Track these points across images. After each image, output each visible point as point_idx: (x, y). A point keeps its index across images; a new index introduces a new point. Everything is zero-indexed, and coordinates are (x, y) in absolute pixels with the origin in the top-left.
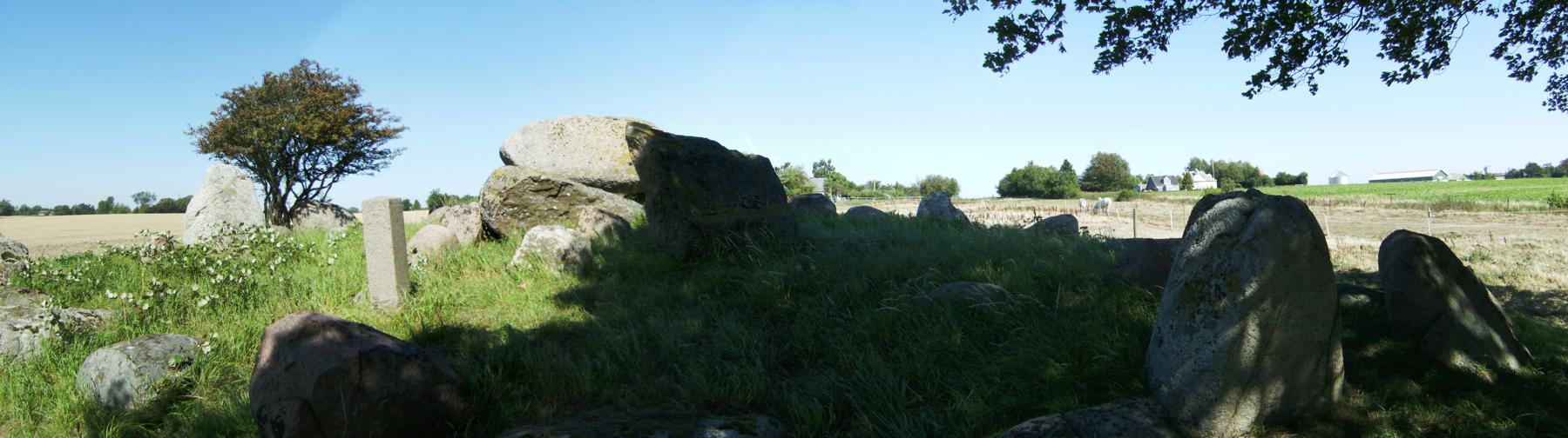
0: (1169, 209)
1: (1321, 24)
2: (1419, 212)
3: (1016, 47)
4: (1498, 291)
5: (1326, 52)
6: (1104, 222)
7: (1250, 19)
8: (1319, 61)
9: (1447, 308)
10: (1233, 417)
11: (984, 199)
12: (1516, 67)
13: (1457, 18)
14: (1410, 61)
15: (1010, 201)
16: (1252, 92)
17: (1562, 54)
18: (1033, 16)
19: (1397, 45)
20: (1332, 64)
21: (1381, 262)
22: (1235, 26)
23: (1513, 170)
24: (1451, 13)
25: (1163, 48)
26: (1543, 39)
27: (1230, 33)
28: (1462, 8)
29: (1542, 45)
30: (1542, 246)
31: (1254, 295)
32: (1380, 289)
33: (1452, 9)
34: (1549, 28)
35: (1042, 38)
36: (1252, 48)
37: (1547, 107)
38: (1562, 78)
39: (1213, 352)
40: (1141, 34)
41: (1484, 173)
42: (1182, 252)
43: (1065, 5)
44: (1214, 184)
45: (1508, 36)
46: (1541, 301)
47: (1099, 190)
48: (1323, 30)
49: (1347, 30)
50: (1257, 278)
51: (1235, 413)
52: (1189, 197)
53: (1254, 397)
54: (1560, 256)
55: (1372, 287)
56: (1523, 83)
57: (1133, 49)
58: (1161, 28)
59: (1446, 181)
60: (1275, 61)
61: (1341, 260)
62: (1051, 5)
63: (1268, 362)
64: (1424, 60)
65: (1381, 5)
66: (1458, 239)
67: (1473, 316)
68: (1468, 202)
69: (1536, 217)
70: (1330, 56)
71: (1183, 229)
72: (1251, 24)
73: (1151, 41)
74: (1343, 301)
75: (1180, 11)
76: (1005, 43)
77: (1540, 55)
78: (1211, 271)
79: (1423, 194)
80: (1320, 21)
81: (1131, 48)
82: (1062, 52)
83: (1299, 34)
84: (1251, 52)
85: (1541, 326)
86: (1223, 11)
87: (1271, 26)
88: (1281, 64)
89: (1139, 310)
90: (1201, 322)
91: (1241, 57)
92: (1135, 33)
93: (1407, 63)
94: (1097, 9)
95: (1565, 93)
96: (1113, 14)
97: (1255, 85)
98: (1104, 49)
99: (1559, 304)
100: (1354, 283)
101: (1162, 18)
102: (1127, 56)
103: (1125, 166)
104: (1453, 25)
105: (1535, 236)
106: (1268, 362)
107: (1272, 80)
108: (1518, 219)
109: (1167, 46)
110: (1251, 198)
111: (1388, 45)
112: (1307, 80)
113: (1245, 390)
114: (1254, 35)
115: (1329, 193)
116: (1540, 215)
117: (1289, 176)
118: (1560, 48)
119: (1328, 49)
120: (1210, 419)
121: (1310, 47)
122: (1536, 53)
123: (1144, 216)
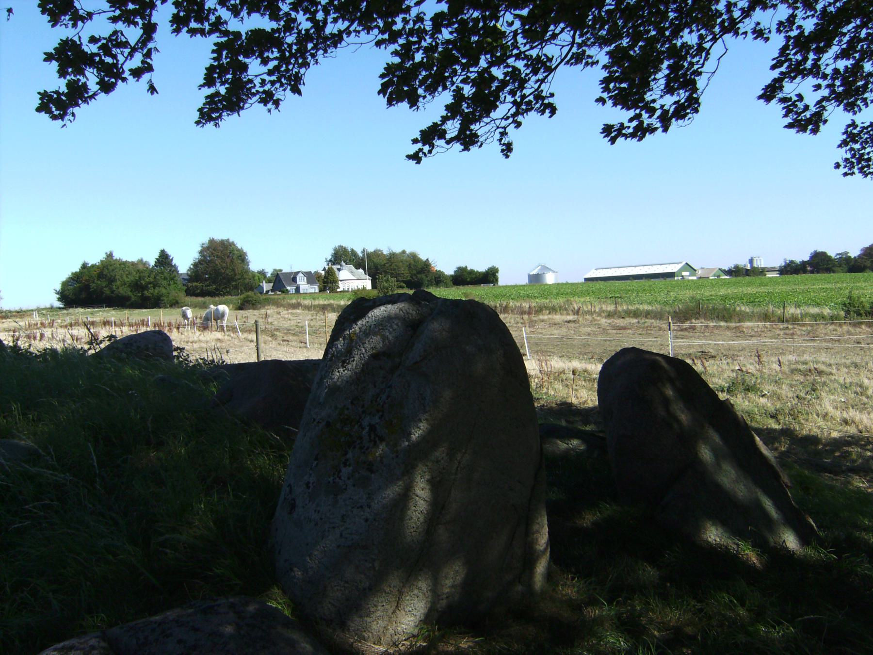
0: (305, 319)
1: (518, 57)
2: (656, 323)
3: (85, 85)
4: (770, 436)
5: (523, 97)
6: (218, 340)
7: (418, 50)
8: (514, 110)
9: (696, 461)
10: (393, 612)
11: (38, 310)
12: (796, 113)
13: (710, 44)
14: (642, 109)
15: (80, 313)
16: (421, 154)
17: (864, 92)
18: (109, 40)
19: (624, 85)
20: (533, 114)
21: (602, 392)
22: (397, 60)
23: (792, 262)
24: (701, 37)
25: (296, 90)
26: (836, 71)
27: (390, 69)
28: (717, 29)
29: (833, 79)
30: (834, 371)
31: (423, 438)
32: (601, 432)
33: (703, 32)
34: (844, 54)
35: (123, 72)
36: (420, 91)
37: (842, 170)
38: (864, 128)
39: (366, 520)
40: (265, 69)
41: (749, 267)
42: (322, 379)
43: (156, 24)
44: (368, 284)
45: (783, 69)
46: (833, 452)
47: (212, 294)
48: (520, 64)
49: (554, 64)
50: (426, 416)
51: (397, 607)
52: (332, 301)
53: (423, 585)
54: (861, 386)
55: (588, 428)
56: (807, 136)
57: (254, 91)
58: (292, 61)
59: (694, 278)
60: (453, 110)
61: (545, 390)
62: (136, 24)
63: (442, 534)
64: (662, 106)
65: (602, 28)
66: (711, 361)
67: (733, 472)
68: (725, 309)
69: (825, 330)
70: (530, 102)
71: (324, 347)
72: (418, 57)
73: (279, 80)
74: (548, 447)
75: (319, 37)
76: (68, 78)
77: (830, 94)
78: (363, 406)
79: (662, 297)
80: (515, 52)
81: (250, 89)
82: (152, 93)
83: (486, 70)
84: (419, 96)
85: (831, 488)
86: (380, 37)
87: (447, 60)
88: (462, 113)
89: (261, 462)
90: (349, 478)
91: (405, 105)
92: (255, 68)
93: (638, 111)
94: (202, 32)
95: (868, 150)
96: (224, 39)
97: (424, 145)
98: (212, 90)
99: (860, 456)
100: (564, 423)
101: (295, 47)
102: (245, 102)
103: (242, 257)
104: (704, 54)
105: (823, 357)
106: (442, 534)
107: (448, 137)
108: (799, 333)
109: (301, 87)
110: (419, 303)
111: (612, 86)
112: (497, 136)
113: (409, 579)
114: (424, 73)
115: (528, 296)
116: (831, 327)
117: (472, 272)
118: (860, 83)
119: (527, 92)
120: (361, 617)
121: (503, 90)
122: (825, 92)
123: (277, 330)
